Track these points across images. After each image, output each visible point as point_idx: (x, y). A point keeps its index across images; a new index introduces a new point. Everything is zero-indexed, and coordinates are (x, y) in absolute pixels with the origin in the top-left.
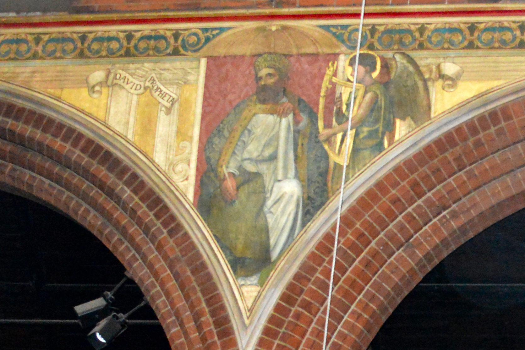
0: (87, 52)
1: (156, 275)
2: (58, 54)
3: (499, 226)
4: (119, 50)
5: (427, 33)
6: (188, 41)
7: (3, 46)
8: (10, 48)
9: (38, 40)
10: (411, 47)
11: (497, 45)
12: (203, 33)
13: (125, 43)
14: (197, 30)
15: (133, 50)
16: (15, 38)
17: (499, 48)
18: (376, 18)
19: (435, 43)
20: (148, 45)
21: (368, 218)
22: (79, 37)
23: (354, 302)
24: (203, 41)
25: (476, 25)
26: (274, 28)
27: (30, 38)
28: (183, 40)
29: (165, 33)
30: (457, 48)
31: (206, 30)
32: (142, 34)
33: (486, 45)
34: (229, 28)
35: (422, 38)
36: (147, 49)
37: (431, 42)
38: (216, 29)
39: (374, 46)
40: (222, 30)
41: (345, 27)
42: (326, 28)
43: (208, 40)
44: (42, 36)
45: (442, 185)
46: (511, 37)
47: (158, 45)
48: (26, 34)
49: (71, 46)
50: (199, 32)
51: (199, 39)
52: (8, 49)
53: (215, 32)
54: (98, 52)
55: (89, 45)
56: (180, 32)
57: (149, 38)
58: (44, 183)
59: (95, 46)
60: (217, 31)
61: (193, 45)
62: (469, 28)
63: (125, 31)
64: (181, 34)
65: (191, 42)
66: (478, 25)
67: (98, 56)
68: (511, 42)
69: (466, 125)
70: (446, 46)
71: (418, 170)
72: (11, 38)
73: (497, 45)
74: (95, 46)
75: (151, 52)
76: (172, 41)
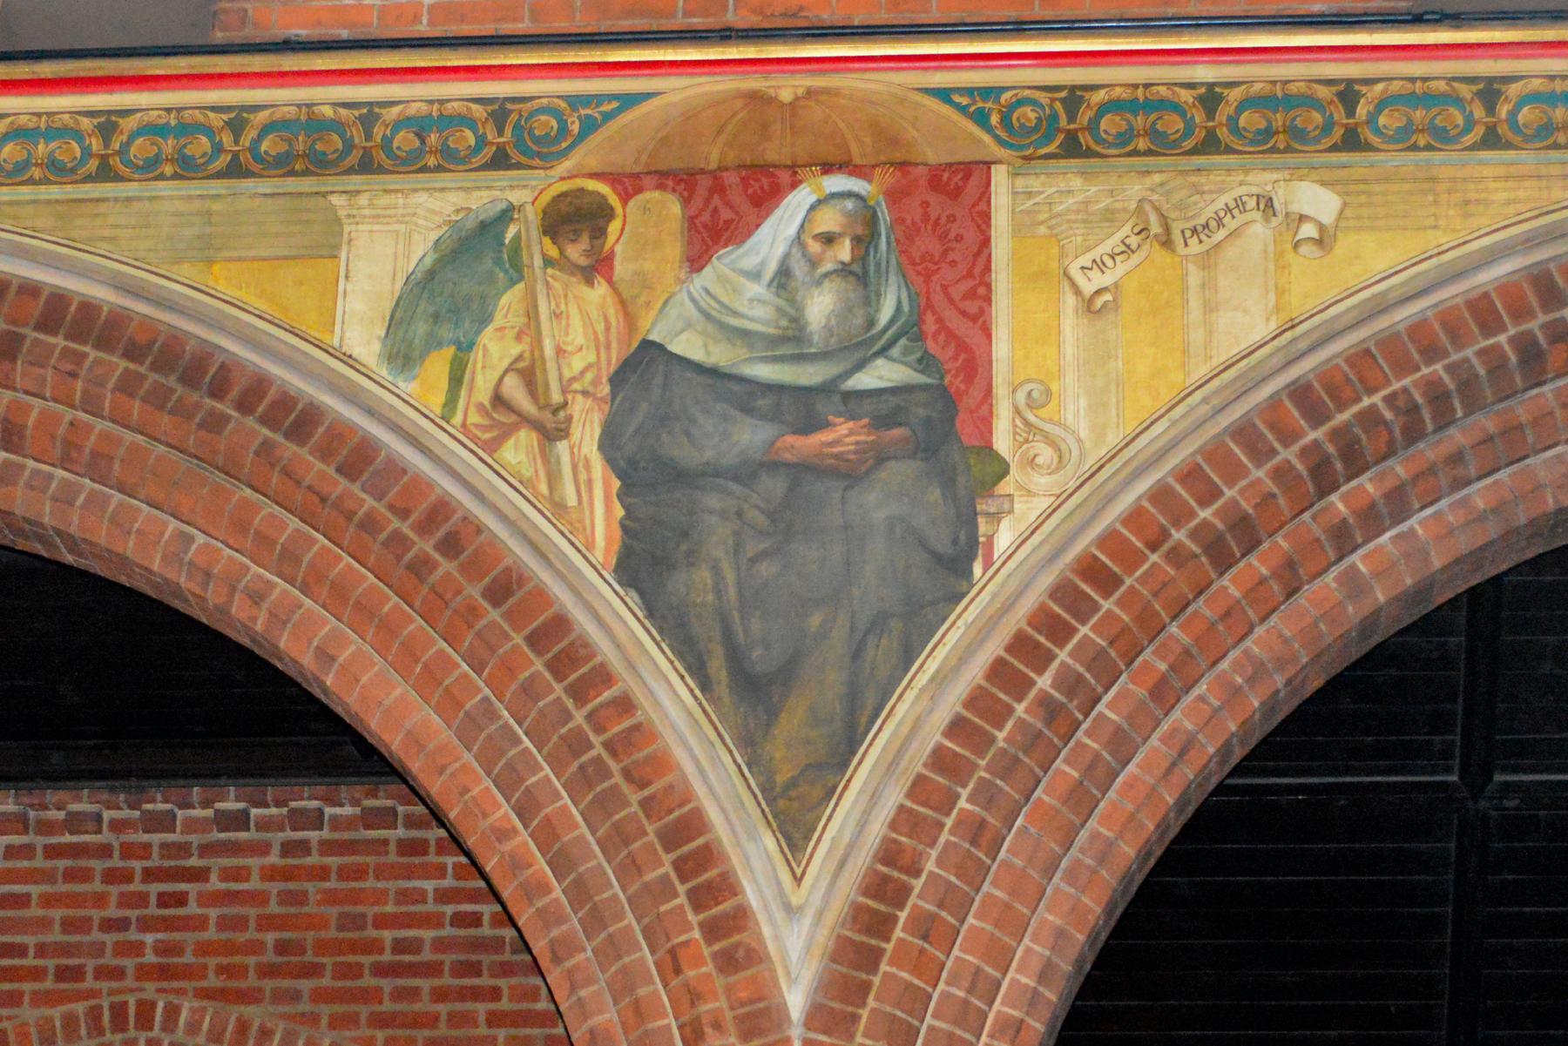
1: (595, 920)
3: (1336, 686)
4: (476, 150)
5: (379, 132)
6: (531, 129)
7: (8, 148)
8: (29, 154)
12: (574, 108)
13: (1199, 117)
14: (556, 100)
15: (1223, 133)
16: (173, 123)
17: (439, 169)
18: (40, 94)
19: (1251, 136)
20: (29, 154)
22: (361, 118)
24: (575, 128)
25: (1079, 93)
28: (517, 126)
30: (200, 175)
31: (574, 101)
32: (1385, 90)
34: (648, 96)
35: (1213, 119)
36: (1269, 133)
37: (1378, 131)
38: (599, 99)
39: (1219, 141)
40: (629, 101)
42: (944, 94)
43: (589, 127)
51: (564, 130)
53: (607, 108)
55: (1514, 113)
56: (509, 106)
57: (1414, 100)
58: (1412, 531)
60: (615, 105)
62: (1063, 101)
64: (512, 111)
70: (1142, 144)
71: (1220, 493)
73: (37, 173)
75: (37, 173)
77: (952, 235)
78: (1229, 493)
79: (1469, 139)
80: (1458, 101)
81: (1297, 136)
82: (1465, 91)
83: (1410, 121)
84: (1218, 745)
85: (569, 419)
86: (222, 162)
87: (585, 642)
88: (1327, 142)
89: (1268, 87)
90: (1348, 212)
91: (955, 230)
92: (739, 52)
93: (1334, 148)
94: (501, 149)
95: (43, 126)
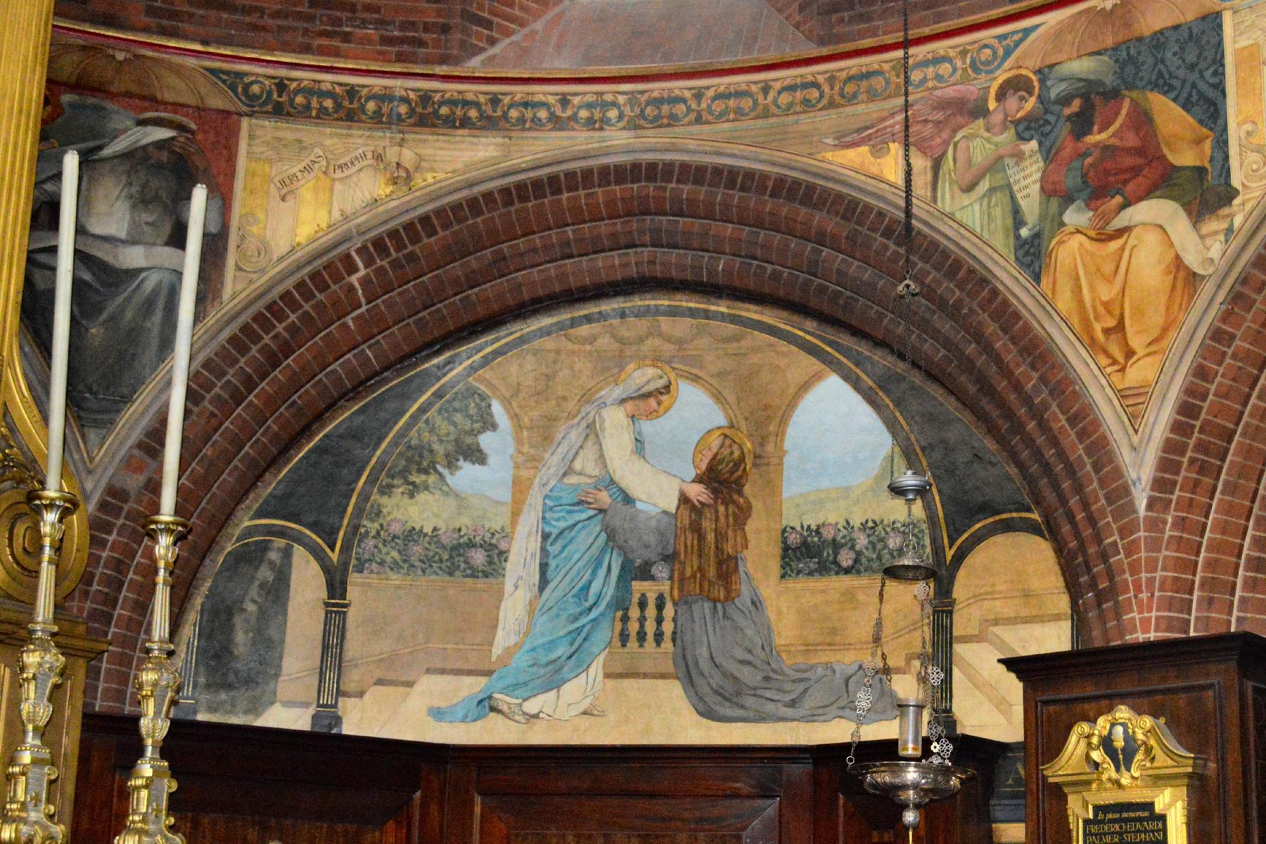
0: (705, 116)
2: (863, 97)
9: (766, 90)
10: (686, 120)
11: (665, 121)
21: (1132, 615)
23: (240, 405)
27: (754, 88)
29: (881, 67)
33: (651, 122)
38: (1014, 33)
40: (1027, 32)
44: (772, 84)
45: (428, 311)
46: (950, 70)
47: (742, 105)
48: (748, 83)
49: (815, 93)
50: (995, 42)
51: (995, 53)
52: (923, 75)
53: (1016, 37)
54: (855, 95)
59: (785, 99)
61: (988, 63)
63: (826, 72)
65: (983, 59)
66: (772, 84)
68: (752, 110)
69: (954, 260)
72: (793, 83)
74: (849, 88)
76: (826, 89)
91: (1141, 59)
94: (422, 116)
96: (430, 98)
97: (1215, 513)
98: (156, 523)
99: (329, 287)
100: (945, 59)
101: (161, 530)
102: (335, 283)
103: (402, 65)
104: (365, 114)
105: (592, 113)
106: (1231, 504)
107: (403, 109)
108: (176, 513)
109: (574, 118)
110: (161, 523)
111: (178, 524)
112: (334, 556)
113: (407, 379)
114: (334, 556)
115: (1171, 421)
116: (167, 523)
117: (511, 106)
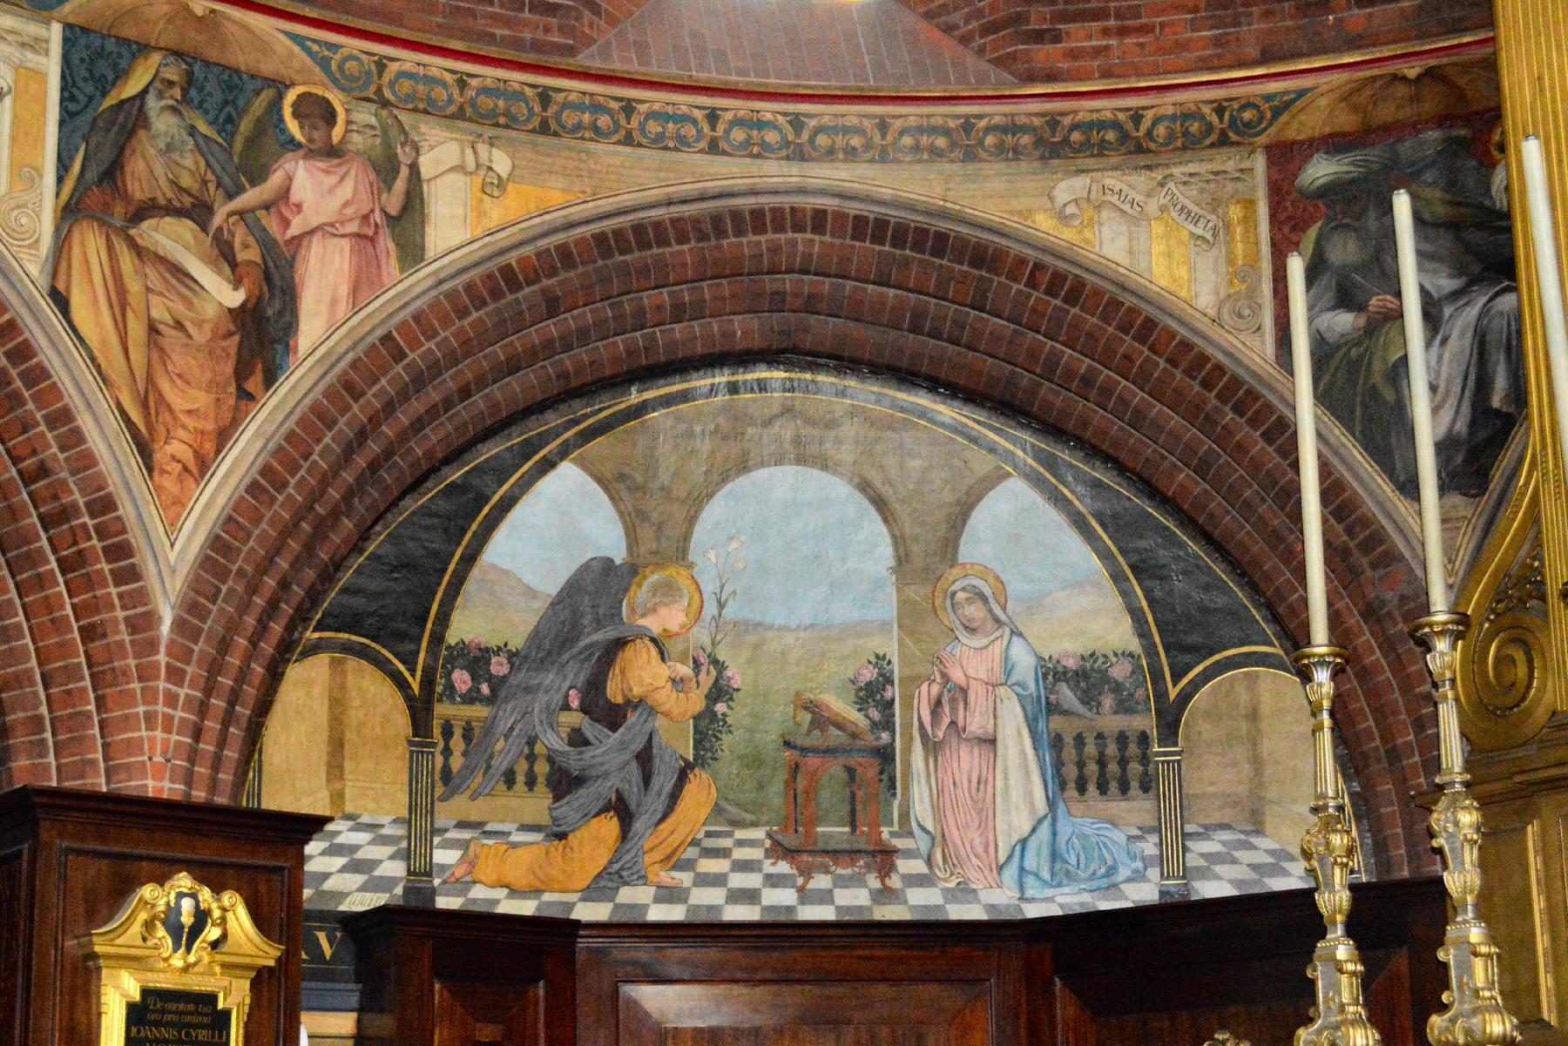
11: (755, 150)
26: (1412, 73)
32: (650, 108)
41: (334, 47)
53: (315, 48)
67: (410, 106)
70: (502, 120)
77: (206, 91)
78: (411, 356)
79: (615, 138)
80: (695, 122)
81: (512, 123)
82: (698, 114)
83: (750, 137)
84: (284, 624)
85: (1090, 710)
86: (452, 109)
87: (339, 378)
88: (615, 138)
89: (1004, 119)
90: (517, 172)
91: (208, 87)
92: (1362, 54)
93: (619, 143)
94: (884, 149)
95: (587, 102)
96: (1058, 123)
97: (53, 570)
98: (1308, 656)
99: (406, 356)
100: (860, 131)
101: (1314, 664)
102: (412, 350)
103: (1104, 81)
104: (1155, 142)
105: (834, 142)
106: (34, 565)
107: (941, 142)
108: (1331, 644)
109: (1066, 141)
110: (1314, 655)
111: (1336, 655)
112: (1173, 693)
113: (528, 459)
114: (1173, 693)
115: (247, 481)
116: (1322, 656)
117: (902, 133)
